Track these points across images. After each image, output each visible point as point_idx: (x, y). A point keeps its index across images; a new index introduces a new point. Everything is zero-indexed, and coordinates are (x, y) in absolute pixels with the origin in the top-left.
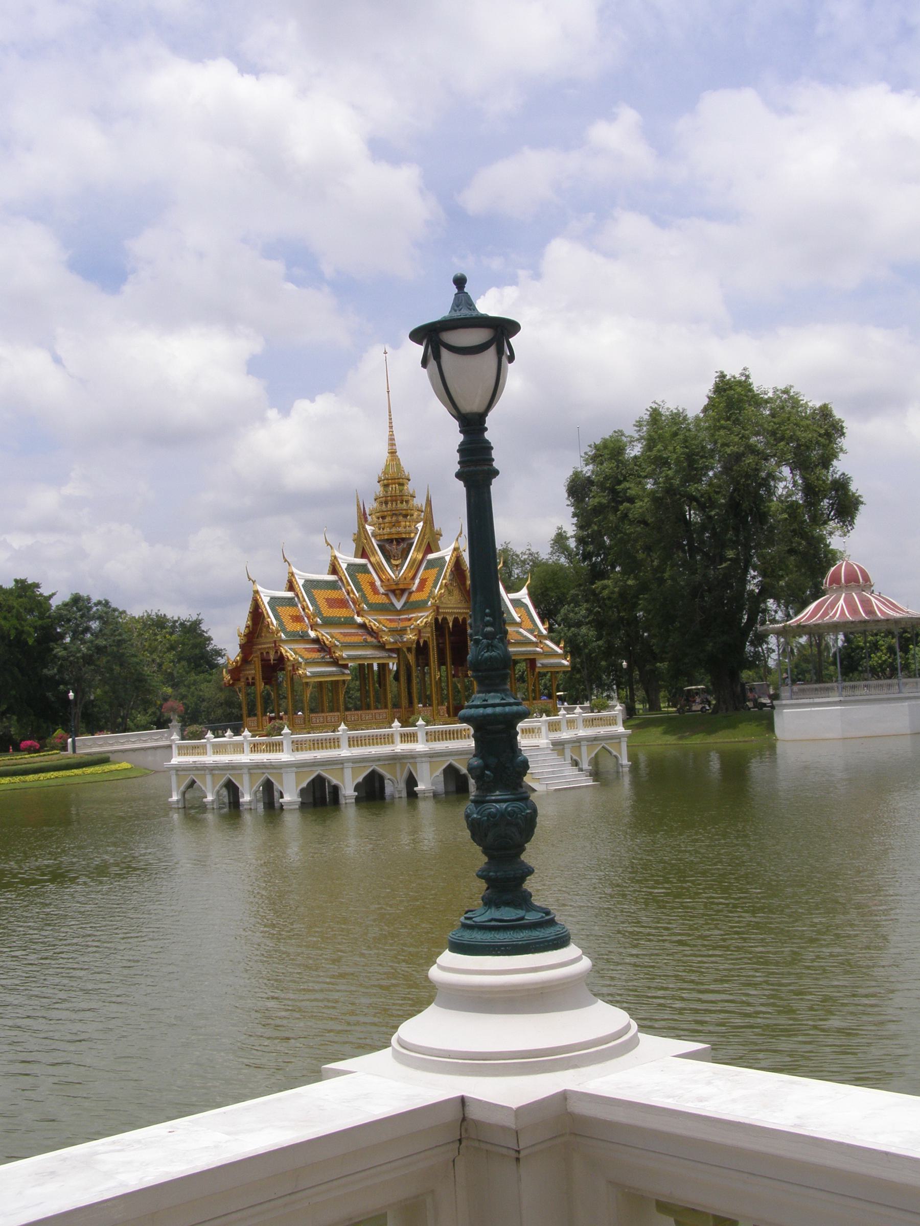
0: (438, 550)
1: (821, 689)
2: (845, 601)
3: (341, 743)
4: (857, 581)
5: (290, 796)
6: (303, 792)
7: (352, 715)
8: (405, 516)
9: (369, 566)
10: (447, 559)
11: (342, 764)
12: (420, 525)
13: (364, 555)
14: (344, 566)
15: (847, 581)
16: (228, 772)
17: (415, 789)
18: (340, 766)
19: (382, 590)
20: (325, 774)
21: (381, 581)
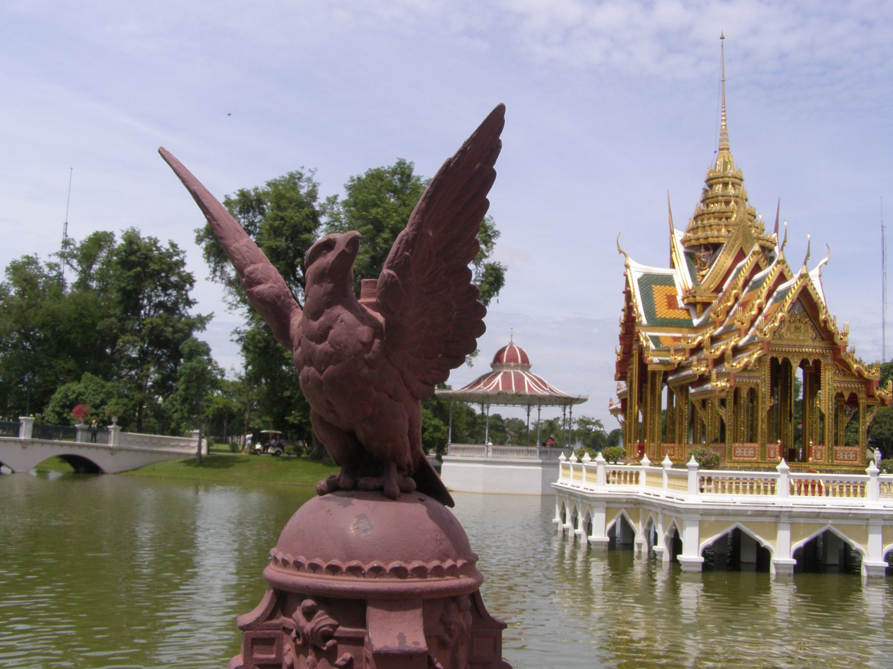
2: (502, 377)
4: (516, 361)
5: (692, 554)
6: (797, 554)
11: (868, 519)
15: (508, 361)
16: (736, 518)
18: (864, 523)
19: (681, 304)
20: (744, 528)
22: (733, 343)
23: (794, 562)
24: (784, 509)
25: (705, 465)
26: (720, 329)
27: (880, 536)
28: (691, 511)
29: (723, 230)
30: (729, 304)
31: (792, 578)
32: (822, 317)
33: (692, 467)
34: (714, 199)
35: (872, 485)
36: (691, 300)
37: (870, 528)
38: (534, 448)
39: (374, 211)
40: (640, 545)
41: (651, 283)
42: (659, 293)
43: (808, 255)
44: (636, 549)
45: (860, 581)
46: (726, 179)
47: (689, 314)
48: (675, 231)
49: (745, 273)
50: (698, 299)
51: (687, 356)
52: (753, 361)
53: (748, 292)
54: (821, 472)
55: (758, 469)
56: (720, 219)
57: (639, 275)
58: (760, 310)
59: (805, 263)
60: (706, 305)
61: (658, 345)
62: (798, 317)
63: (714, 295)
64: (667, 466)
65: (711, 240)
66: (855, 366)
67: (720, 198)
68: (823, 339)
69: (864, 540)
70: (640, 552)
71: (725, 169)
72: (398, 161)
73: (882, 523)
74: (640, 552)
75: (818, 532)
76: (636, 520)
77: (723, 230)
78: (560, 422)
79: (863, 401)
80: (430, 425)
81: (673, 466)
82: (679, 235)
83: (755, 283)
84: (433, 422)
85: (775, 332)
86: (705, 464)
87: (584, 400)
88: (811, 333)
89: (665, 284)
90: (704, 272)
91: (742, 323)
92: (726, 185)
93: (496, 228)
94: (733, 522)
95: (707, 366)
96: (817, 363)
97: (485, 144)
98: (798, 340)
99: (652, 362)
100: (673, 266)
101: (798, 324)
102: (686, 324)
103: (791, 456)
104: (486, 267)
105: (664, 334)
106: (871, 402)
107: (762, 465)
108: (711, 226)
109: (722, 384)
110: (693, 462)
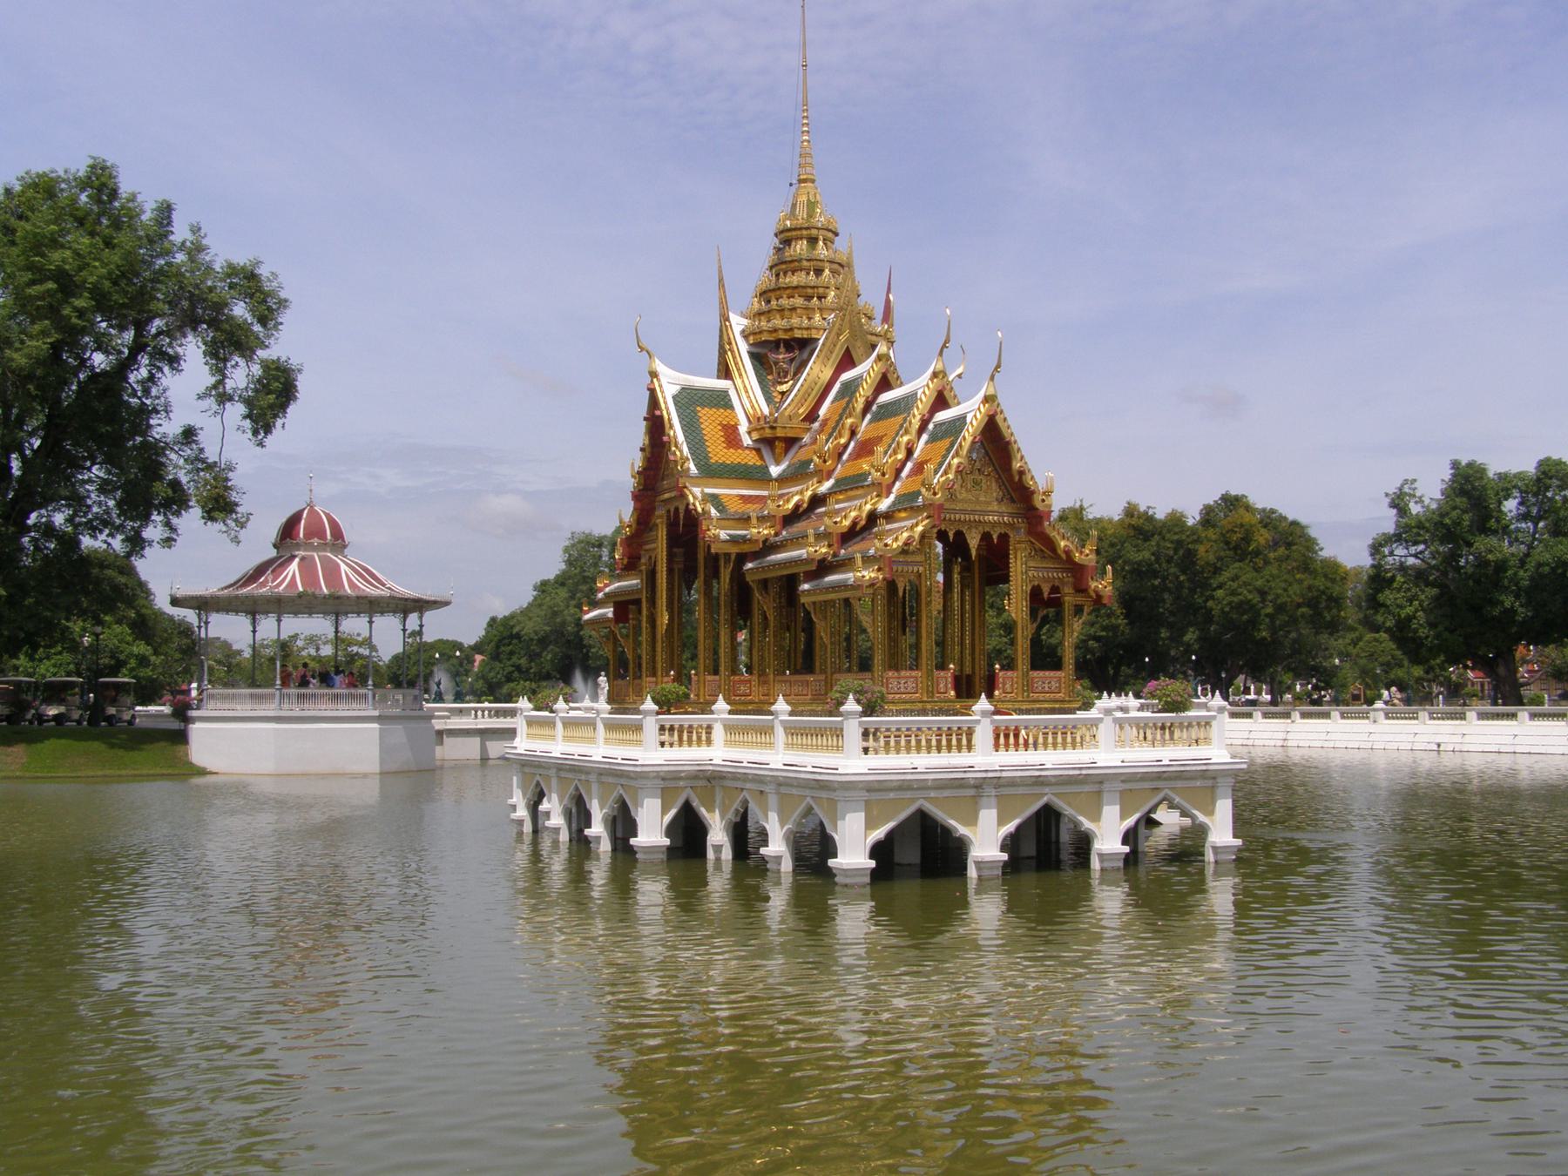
1: (353, 697)
4: (322, 535)
5: (853, 852)
13: (725, 372)
15: (308, 535)
17: (633, 841)
22: (868, 507)
23: (872, 864)
24: (990, 775)
25: (869, 710)
26: (827, 485)
27: (1117, 808)
28: (848, 786)
29: (817, 317)
30: (843, 441)
31: (868, 890)
32: (1016, 465)
33: (850, 714)
34: (793, 266)
35: (983, 735)
36: (768, 433)
38: (361, 691)
39: (56, 256)
40: (718, 849)
41: (695, 403)
42: (709, 419)
43: (999, 366)
44: (711, 854)
46: (814, 232)
47: (762, 458)
48: (732, 316)
49: (864, 391)
50: (780, 433)
51: (778, 527)
52: (917, 536)
53: (871, 422)
54: (1021, 712)
55: (924, 712)
56: (809, 298)
57: (675, 389)
58: (910, 452)
59: (992, 378)
60: (790, 442)
61: (721, 508)
62: (978, 465)
63: (806, 425)
64: (783, 713)
65: (798, 334)
66: (1062, 544)
67: (805, 263)
68: (1012, 501)
69: (972, 820)
70: (718, 859)
71: (811, 215)
72: (91, 162)
74: (718, 859)
76: (710, 810)
77: (817, 317)
78: (300, 643)
79: (1069, 599)
80: (131, 655)
81: (791, 714)
82: (738, 323)
83: (880, 407)
84: (135, 650)
85: (948, 488)
86: (666, 704)
87: (447, 603)
88: (995, 492)
89: (717, 406)
90: (784, 388)
91: (883, 474)
92: (813, 241)
93: (283, 295)
94: (913, 800)
95: (830, 546)
96: (1004, 538)
98: (978, 502)
99: (716, 537)
100: (725, 372)
101: (976, 476)
102: (756, 476)
104: (267, 366)
105: (729, 492)
106: (1080, 599)
107: (929, 706)
108: (794, 309)
109: (869, 574)
110: (851, 705)
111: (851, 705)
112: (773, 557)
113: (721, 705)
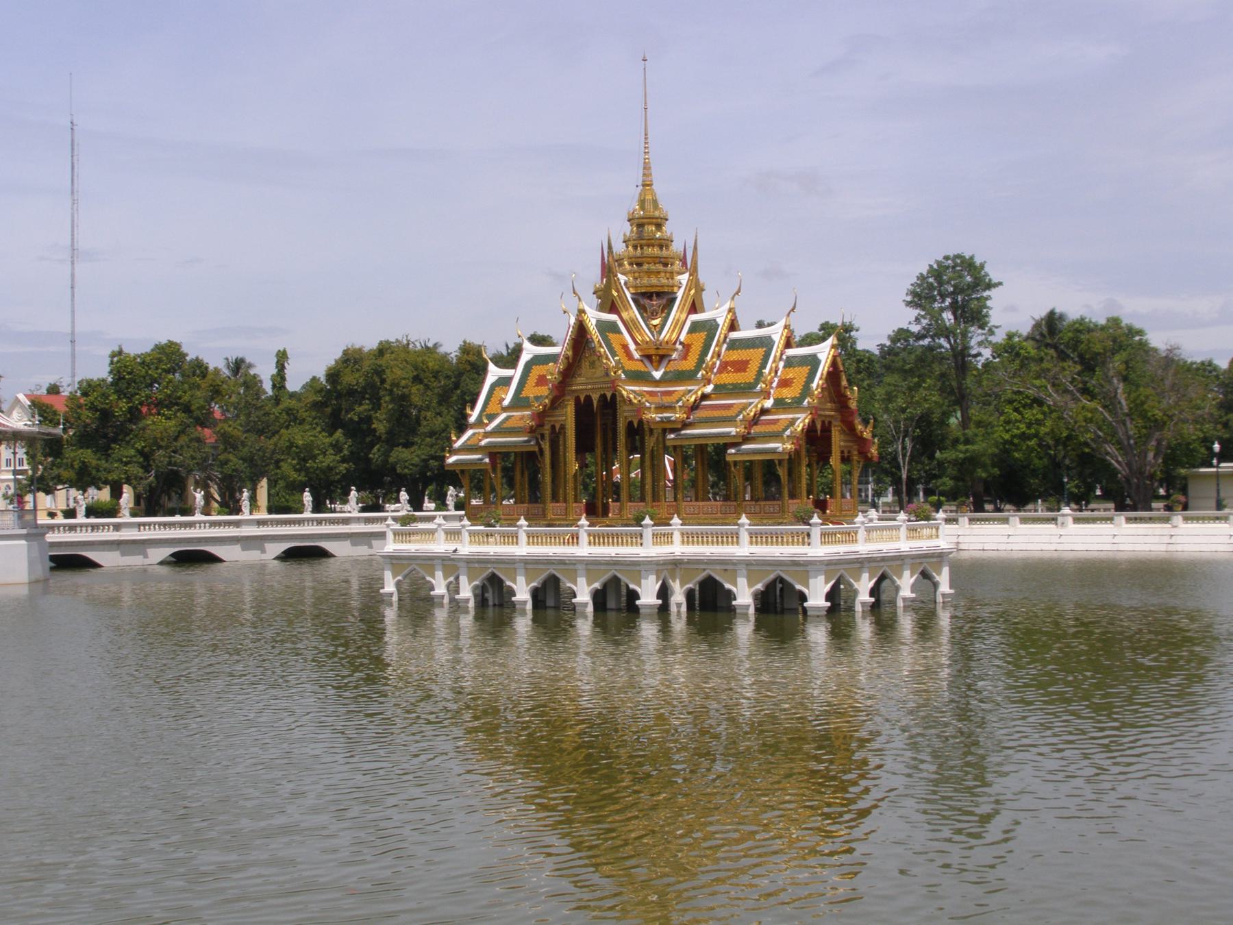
0: (703, 311)
1: (549, 535)
3: (644, 541)
7: (689, 506)
8: (666, 265)
9: (620, 324)
10: (720, 321)
12: (684, 278)
13: (613, 309)
14: (594, 322)
19: (637, 356)
20: (619, 575)
21: (636, 343)
28: (740, 562)
33: (816, 524)
37: (811, 574)
45: (854, 617)
70: (679, 612)
73: (656, 568)
74: (679, 612)
75: (771, 577)
96: (830, 423)
97: (1000, 284)
103: (821, 506)
111: (647, 521)
112: (688, 432)
113: (676, 520)
